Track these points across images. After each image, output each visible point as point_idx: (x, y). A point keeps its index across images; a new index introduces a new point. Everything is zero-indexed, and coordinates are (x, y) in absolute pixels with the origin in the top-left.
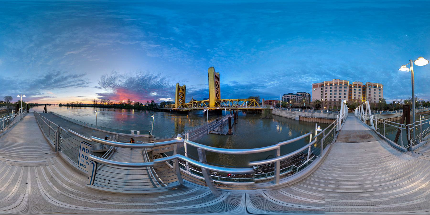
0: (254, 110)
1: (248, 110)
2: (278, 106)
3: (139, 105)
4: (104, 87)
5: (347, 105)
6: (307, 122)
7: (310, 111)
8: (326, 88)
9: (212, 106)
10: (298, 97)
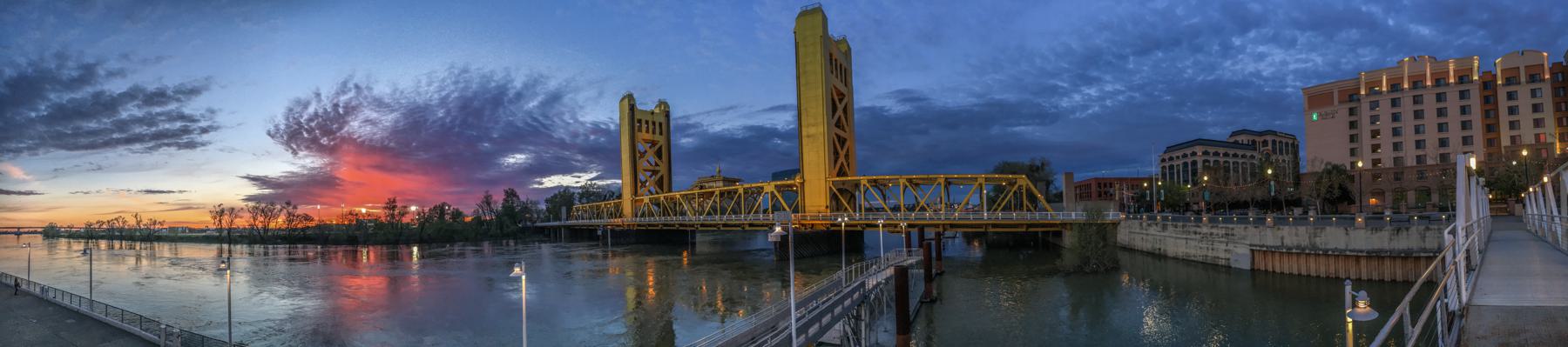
0: (1024, 230)
1: (991, 230)
2: (1142, 204)
3: (447, 217)
4: (292, 148)
5: (1482, 180)
6: (1291, 274)
7: (1303, 220)
8: (1374, 105)
9: (815, 209)
10: (1235, 155)
